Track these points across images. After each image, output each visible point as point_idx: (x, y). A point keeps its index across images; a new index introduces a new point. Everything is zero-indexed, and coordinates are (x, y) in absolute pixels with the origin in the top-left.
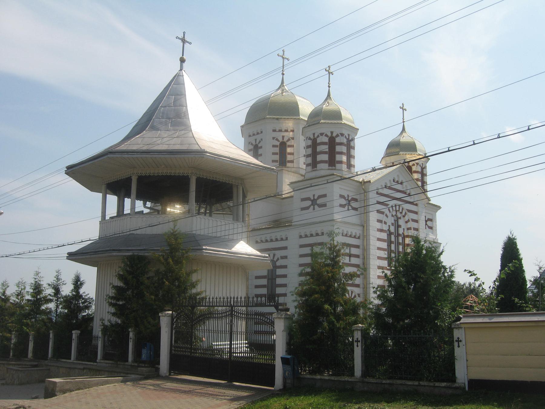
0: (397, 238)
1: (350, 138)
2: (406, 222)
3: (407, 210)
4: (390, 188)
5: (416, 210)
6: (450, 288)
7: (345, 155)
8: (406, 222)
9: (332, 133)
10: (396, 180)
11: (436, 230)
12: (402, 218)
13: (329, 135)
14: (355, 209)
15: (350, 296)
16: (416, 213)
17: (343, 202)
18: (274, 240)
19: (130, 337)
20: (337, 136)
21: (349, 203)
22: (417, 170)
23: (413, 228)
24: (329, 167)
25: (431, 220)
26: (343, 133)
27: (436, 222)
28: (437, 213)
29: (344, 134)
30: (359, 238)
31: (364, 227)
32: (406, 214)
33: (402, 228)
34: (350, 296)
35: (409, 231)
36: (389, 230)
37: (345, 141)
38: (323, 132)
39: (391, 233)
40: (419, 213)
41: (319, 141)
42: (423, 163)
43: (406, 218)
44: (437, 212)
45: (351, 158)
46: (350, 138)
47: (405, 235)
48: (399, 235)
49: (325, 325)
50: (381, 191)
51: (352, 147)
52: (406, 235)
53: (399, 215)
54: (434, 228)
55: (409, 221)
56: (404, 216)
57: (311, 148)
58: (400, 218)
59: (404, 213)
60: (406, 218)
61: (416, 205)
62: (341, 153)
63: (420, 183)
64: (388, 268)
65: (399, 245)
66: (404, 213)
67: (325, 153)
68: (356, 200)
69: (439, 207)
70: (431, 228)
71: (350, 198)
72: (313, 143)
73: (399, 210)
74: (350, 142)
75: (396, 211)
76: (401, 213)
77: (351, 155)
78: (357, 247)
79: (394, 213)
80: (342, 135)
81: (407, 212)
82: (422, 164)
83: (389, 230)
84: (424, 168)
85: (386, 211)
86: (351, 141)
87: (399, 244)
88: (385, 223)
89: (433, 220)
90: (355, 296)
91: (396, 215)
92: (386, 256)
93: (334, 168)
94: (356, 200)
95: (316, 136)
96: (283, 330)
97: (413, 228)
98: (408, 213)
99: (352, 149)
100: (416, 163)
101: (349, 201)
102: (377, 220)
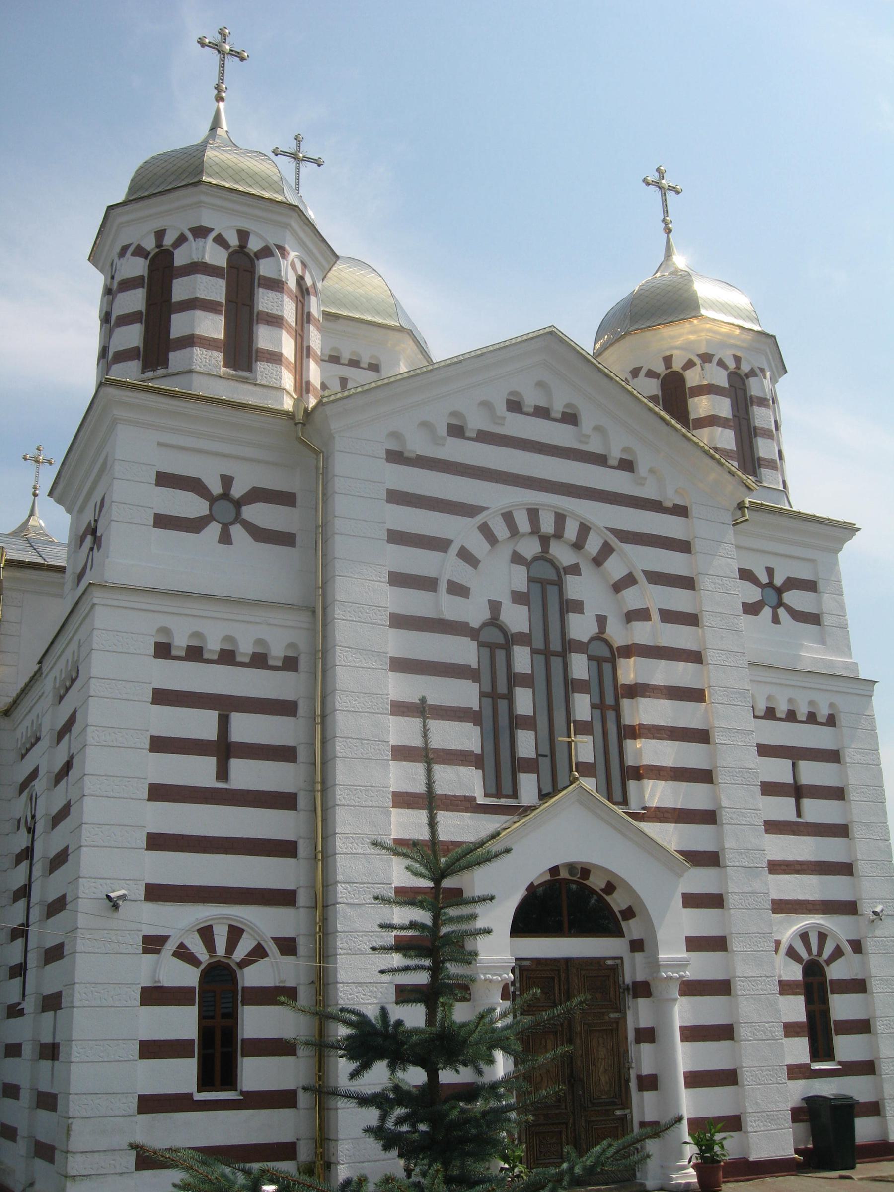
0: (556, 662)
1: (254, 245)
2: (618, 587)
3: (615, 532)
4: (484, 437)
5: (695, 723)
6: (469, 957)
7: (729, 427)
8: (618, 587)
9: (160, 235)
10: (531, 399)
11: (844, 627)
12: (586, 568)
13: (660, 368)
14: (285, 539)
15: (815, 950)
16: (684, 547)
17: (754, 594)
18: (778, 715)
19: (631, 992)
20: (181, 240)
21: (238, 513)
22: (705, 383)
23: (661, 611)
24: (143, 373)
25: (810, 586)
26: (206, 224)
27: (842, 595)
28: (840, 555)
29: (210, 230)
30: (290, 664)
31: (314, 612)
32: (607, 550)
33: (590, 612)
34: (815, 950)
35: (637, 625)
36: (494, 622)
37: (217, 257)
38: (641, 366)
39: (512, 635)
40: (697, 546)
41: (180, 258)
42: (738, 354)
43: (615, 568)
44: (841, 549)
45: (756, 436)
46: (254, 245)
47: (615, 645)
48: (569, 646)
49: (392, 1095)
50: (418, 445)
51: (755, 400)
52: (618, 648)
53: (563, 554)
54: (827, 620)
55: (629, 580)
56: (598, 561)
57: (143, 287)
58: (574, 570)
59: (593, 545)
60: (615, 568)
61: (681, 511)
62: (276, 321)
63: (726, 438)
64: (481, 800)
65: (573, 692)
66: (593, 545)
67: (210, 306)
68: (286, 499)
69: (849, 530)
70: (814, 619)
71: (778, 581)
72: (152, 268)
73: (559, 535)
74: (744, 384)
75: (545, 541)
76: (578, 546)
77: (755, 427)
78: (286, 708)
79: (530, 548)
80: (200, 232)
81: (614, 541)
82: (737, 359)
83: (494, 622)
84: (747, 376)
85: (478, 545)
86: (258, 259)
87: (572, 686)
88: (458, 590)
89: (821, 585)
90: (838, 953)
91: (544, 557)
92: (639, 743)
93: (161, 372)
94: (286, 499)
95: (168, 241)
96: (141, 1147)
97: (661, 611)
98: (624, 545)
99: (755, 407)
100: (698, 355)
101: (779, 591)
102: (391, 573)
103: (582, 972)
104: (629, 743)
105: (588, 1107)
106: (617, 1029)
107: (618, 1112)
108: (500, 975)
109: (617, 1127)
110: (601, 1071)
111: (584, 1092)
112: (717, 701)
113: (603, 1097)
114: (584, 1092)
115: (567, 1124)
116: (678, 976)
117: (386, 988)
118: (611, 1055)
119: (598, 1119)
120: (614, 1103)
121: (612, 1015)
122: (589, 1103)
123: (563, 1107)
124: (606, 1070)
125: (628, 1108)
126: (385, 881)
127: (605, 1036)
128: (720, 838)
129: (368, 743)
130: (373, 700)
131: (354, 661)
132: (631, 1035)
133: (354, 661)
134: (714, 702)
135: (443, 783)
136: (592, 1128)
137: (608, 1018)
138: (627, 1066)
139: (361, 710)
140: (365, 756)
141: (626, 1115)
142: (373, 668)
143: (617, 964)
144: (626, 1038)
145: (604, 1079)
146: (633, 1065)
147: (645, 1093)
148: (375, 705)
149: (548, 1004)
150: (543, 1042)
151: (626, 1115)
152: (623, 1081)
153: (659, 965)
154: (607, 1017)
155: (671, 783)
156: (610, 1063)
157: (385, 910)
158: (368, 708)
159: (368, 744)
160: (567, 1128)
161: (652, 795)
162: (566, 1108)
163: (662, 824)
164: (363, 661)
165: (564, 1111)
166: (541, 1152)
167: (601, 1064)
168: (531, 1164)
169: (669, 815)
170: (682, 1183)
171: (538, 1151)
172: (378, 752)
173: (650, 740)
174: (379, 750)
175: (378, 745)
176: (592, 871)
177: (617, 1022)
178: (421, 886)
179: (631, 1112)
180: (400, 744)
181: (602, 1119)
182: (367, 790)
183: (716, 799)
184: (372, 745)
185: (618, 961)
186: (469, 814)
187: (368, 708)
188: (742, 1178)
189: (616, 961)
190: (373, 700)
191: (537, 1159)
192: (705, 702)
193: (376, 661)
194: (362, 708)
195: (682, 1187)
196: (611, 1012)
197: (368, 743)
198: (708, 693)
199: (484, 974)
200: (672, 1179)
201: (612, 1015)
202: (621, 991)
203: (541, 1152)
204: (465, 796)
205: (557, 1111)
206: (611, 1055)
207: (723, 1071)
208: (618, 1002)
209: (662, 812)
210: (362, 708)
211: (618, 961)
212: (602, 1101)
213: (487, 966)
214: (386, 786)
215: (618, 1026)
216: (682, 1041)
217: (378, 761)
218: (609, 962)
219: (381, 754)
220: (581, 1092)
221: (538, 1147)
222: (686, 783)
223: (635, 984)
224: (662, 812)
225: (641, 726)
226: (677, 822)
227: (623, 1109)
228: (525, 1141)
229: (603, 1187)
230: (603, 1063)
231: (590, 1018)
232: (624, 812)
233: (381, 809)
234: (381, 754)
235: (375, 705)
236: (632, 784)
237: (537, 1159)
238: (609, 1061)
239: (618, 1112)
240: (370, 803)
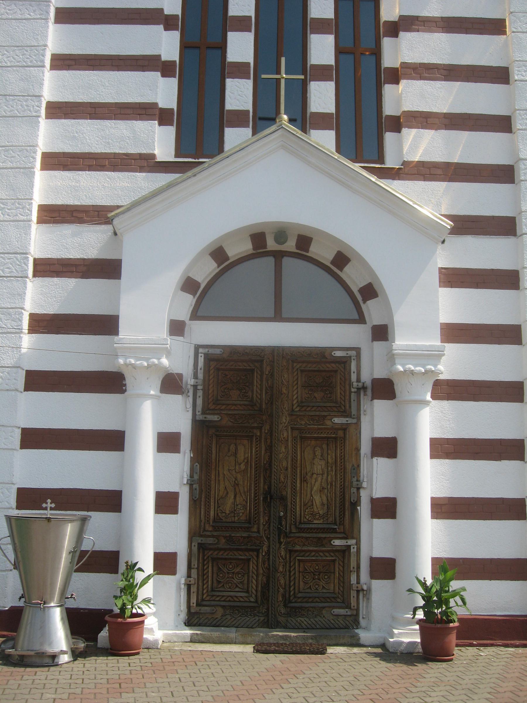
103: (295, 364)
104: (388, 89)
105: (291, 532)
106: (344, 438)
107: (337, 542)
108: (147, 360)
109: (334, 561)
110: (315, 488)
111: (285, 514)
112: (520, 30)
113: (315, 522)
114: (285, 514)
115: (258, 551)
116: (423, 370)
117: (8, 373)
118: (332, 470)
119: (305, 548)
120: (334, 531)
121: (337, 420)
122: (293, 527)
123: (255, 529)
124: (323, 488)
125: (353, 538)
126: (19, 251)
127: (324, 446)
128: (517, 201)
129: (15, 99)
130: (25, 52)
131: (7, 13)
132: (365, 447)
133: (7, 13)
134: (515, 30)
135: (112, 140)
136: (295, 558)
137: (331, 423)
138: (355, 483)
139: (9, 64)
140: (9, 114)
141: (349, 547)
142: (30, 19)
143: (350, 357)
144: (358, 450)
145: (317, 499)
146: (365, 485)
147: (374, 520)
148: (28, 58)
149: (242, 403)
150: (232, 447)
151: (349, 547)
152: (347, 504)
153: (394, 355)
154: (328, 423)
155: (443, 133)
156: (329, 480)
157: (15, 284)
158: (18, 62)
159: (13, 100)
160: (258, 556)
161: (414, 147)
162: (258, 532)
163: (427, 183)
164: (19, 12)
165: (255, 535)
166: (219, 582)
167: (316, 480)
168: (203, 595)
169: (439, 172)
170: (403, 642)
171: (215, 581)
172: (26, 108)
173: (415, 81)
174: (27, 106)
175: (26, 101)
176: (315, 238)
177: (344, 428)
178: (72, 257)
179: (358, 544)
180: (61, 100)
181: (311, 548)
182: (7, 151)
183: (514, 151)
184: (19, 100)
185: (353, 353)
186: (144, 174)
187: (18, 62)
188: (518, 642)
189: (348, 352)
190: (25, 52)
191: (213, 590)
192: (506, 34)
193: (34, 11)
194: (11, 62)
195: (402, 648)
196: (335, 416)
197: (15, 99)
198: (509, 23)
199: (126, 357)
200: (392, 635)
201: (337, 420)
202: (353, 390)
203: (219, 582)
204: (140, 154)
205: (245, 534)
206: (332, 470)
207: (502, 500)
208: (348, 405)
209: (429, 168)
210: (11, 62)
211: (353, 353)
212: (313, 526)
213: (130, 348)
214: (31, 144)
215: (345, 434)
216: (432, 456)
217: (25, 119)
218: (338, 354)
219: (30, 111)
220: (282, 514)
221: (215, 575)
222: (468, 132)
223: (375, 382)
224: (429, 168)
225: (404, 65)
226: (451, 179)
227: (346, 538)
228: (196, 566)
229: (293, 634)
230: (319, 479)
231: (303, 423)
232: (363, 167)
233: (22, 170)
234: (30, 111)
235: (28, 58)
236: (389, 137)
237: (213, 590)
238: (329, 477)
239: (337, 542)
240: (9, 165)
